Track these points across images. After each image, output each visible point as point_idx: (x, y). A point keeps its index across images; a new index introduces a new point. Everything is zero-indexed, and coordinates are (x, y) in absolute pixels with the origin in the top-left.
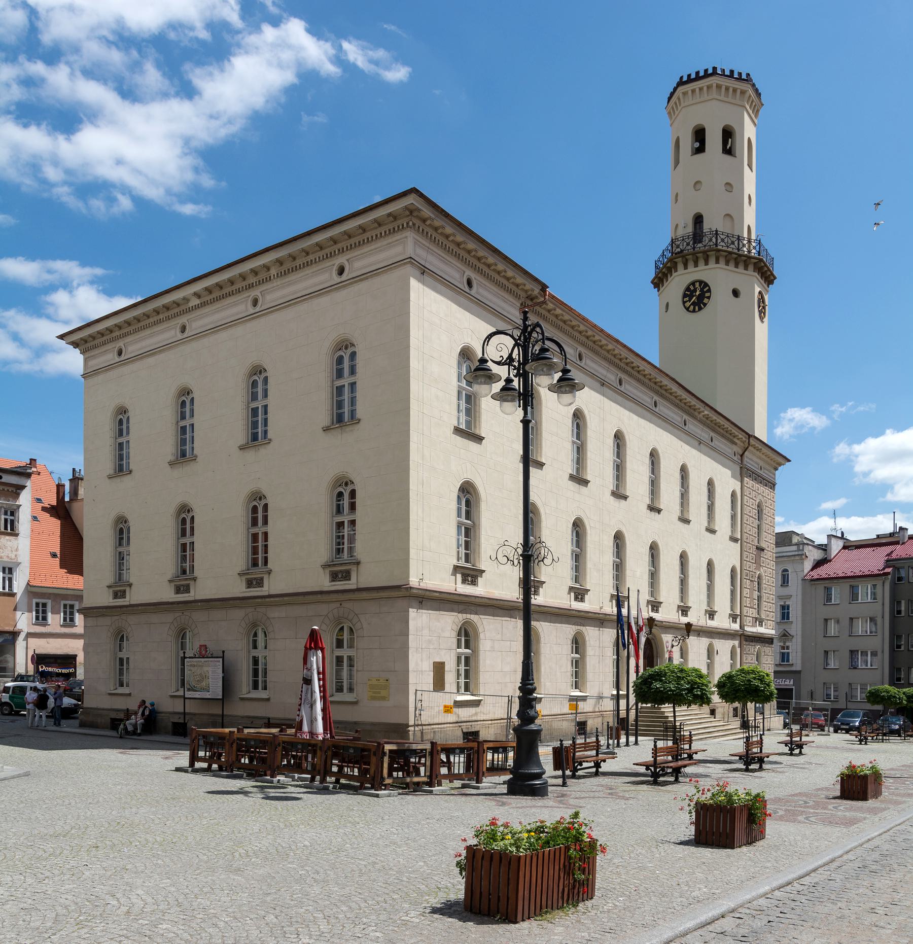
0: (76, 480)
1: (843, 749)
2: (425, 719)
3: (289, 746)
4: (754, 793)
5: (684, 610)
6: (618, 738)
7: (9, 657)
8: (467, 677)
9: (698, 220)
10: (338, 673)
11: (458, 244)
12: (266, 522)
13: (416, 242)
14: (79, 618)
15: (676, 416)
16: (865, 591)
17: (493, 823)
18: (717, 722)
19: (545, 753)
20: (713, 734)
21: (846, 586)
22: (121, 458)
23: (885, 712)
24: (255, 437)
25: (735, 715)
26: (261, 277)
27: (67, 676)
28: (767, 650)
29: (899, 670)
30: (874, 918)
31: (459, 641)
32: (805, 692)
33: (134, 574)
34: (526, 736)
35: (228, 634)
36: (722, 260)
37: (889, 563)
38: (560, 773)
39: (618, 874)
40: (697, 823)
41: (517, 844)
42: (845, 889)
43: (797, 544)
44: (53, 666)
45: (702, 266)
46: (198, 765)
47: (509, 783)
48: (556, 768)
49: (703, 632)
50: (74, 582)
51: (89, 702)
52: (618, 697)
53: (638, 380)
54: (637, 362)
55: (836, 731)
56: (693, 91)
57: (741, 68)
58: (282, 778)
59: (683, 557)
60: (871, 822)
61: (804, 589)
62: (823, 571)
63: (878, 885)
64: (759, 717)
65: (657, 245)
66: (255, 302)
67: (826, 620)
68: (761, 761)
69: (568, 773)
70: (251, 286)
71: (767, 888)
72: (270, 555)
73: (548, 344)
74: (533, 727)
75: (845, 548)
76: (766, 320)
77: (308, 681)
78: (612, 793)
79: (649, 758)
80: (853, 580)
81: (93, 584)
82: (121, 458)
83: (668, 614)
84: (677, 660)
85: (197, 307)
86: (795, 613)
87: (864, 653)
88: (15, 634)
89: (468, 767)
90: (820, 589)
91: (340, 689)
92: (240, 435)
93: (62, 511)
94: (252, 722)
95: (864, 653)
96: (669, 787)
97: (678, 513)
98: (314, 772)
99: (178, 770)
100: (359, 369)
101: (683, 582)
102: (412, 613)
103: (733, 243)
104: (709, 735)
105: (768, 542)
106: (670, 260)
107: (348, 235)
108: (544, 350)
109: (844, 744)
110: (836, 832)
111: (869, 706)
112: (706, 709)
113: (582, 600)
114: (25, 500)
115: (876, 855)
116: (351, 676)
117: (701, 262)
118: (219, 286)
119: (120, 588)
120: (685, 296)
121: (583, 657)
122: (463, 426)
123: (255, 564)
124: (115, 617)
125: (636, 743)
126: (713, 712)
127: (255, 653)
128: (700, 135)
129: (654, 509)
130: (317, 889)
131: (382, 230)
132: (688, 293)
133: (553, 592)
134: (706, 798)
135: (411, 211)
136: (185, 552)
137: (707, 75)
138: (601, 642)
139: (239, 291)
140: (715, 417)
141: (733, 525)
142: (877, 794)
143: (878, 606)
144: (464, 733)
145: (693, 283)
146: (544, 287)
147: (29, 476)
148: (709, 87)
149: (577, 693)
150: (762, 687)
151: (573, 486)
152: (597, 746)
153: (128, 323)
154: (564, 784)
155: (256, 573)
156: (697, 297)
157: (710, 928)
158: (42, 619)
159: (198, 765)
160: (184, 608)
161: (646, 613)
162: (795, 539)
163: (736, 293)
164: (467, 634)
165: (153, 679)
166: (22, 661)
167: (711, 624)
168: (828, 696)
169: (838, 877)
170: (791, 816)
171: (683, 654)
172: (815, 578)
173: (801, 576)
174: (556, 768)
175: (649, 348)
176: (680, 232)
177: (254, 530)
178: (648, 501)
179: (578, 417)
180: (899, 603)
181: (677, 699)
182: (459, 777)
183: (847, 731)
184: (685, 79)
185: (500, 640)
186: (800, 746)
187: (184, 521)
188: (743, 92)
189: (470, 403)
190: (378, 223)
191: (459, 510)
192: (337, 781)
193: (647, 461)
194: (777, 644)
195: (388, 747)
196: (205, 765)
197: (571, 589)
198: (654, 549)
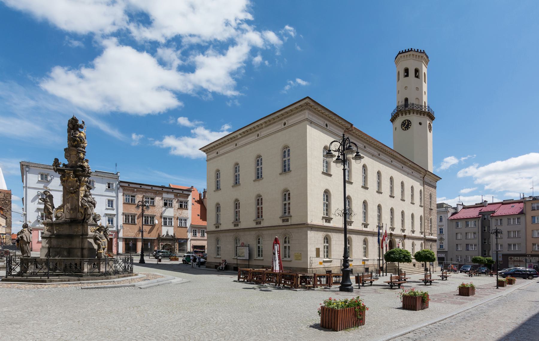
0: (205, 192)
1: (463, 278)
2: (313, 266)
3: (268, 275)
4: (424, 292)
5: (403, 231)
6: (380, 273)
7: (185, 246)
8: (327, 253)
9: (406, 100)
10: (285, 251)
11: (323, 113)
13: (309, 114)
14: (206, 234)
15: (399, 165)
16: (471, 224)
17: (330, 299)
18: (416, 269)
19: (352, 278)
20: (413, 273)
21: (464, 222)
22: (218, 185)
23: (480, 266)
24: (258, 177)
25: (423, 266)
26: (260, 127)
27: (202, 252)
28: (434, 244)
29: (485, 251)
30: (464, 335)
31: (324, 241)
32: (449, 258)
33: (221, 221)
34: (346, 272)
35: (250, 239)
36: (415, 113)
37: (480, 213)
38: (358, 284)
39: (374, 318)
40: (403, 302)
41: (337, 306)
42: (455, 325)
43: (445, 207)
44: (198, 249)
45: (408, 115)
46: (240, 280)
47: (340, 287)
48: (356, 283)
49: (410, 238)
50: (204, 223)
51: (209, 260)
52: (379, 260)
53: (385, 154)
54: (385, 148)
55: (461, 272)
56: (404, 56)
57: (421, 48)
58: (266, 284)
59: (403, 213)
60: (469, 304)
61: (448, 224)
62: (455, 217)
63: (468, 324)
64: (431, 267)
65: (392, 108)
66: (258, 135)
67: (457, 234)
68: (431, 282)
69: (361, 284)
70: (257, 130)
71: (427, 324)
72: (263, 214)
73: (351, 144)
74: (348, 269)
75: (463, 208)
76: (432, 132)
77: (274, 254)
78: (376, 291)
79: (389, 280)
80: (467, 220)
81: (209, 224)
82: (218, 185)
83: (397, 231)
84: (401, 247)
85: (240, 138)
86: (445, 231)
87: (472, 245)
88: (187, 239)
89: (327, 282)
90: (454, 223)
91: (285, 257)
92: (254, 176)
93: (201, 202)
94: (258, 266)
95: (472, 245)
96: (396, 290)
97: (401, 198)
98: (276, 282)
99: (234, 281)
100: (291, 154)
101: (403, 221)
102: (309, 232)
104: (413, 273)
105: (434, 207)
106: (396, 113)
107: (287, 113)
108: (350, 146)
109: (463, 277)
110: (455, 306)
111: (473, 264)
112: (412, 264)
113: (367, 227)
114: (190, 199)
115: (469, 315)
116: (289, 253)
117: (408, 114)
118: (247, 131)
119: (217, 225)
120: (402, 125)
121: (367, 246)
122: (325, 172)
123: (258, 217)
124: (216, 234)
125: (386, 275)
126: (414, 265)
127: (259, 245)
128: (407, 71)
129: (392, 196)
130: (274, 318)
131: (298, 110)
132: (403, 124)
133: (357, 224)
134: (406, 293)
135: (307, 104)
136: (237, 213)
137: (409, 51)
138: (373, 241)
139: (253, 132)
140: (413, 165)
141: (421, 201)
142: (473, 294)
143: (477, 229)
144: (327, 271)
145: (405, 121)
146: (352, 125)
147: (191, 191)
148: (410, 55)
149: (365, 258)
150: (431, 257)
151: (363, 190)
152: (371, 276)
153: (220, 144)
154: (359, 288)
155: (259, 220)
156: (406, 125)
157: (404, 336)
158: (195, 235)
159: (240, 280)
160: (237, 231)
161: (389, 232)
162: (445, 206)
163: (420, 124)
164: (327, 239)
165: (228, 254)
166: (189, 248)
167: (413, 235)
168: (458, 260)
169: (454, 321)
170: (439, 301)
171: (403, 245)
172: (452, 220)
173: (447, 218)
174: (356, 283)
175: (390, 143)
176: (400, 104)
177: (258, 207)
178: (390, 194)
179: (364, 167)
180: (485, 227)
181: (400, 260)
182: (323, 285)
183: (465, 273)
185: (337, 241)
186: (446, 277)
187: (237, 204)
188: (422, 57)
189: (327, 165)
190: (297, 108)
191: (324, 198)
192: (284, 286)
193: (389, 181)
194: (438, 242)
195: (300, 275)
196: (243, 280)
197: (363, 224)
198: (392, 210)
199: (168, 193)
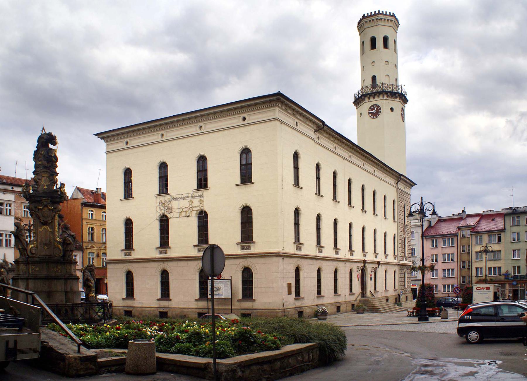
9: (374, 78)
103: (390, 88)
132: (371, 108)
145: (373, 106)
146: (323, 123)
156: (375, 112)
163: (392, 109)
184: (366, 15)
188: (391, 21)
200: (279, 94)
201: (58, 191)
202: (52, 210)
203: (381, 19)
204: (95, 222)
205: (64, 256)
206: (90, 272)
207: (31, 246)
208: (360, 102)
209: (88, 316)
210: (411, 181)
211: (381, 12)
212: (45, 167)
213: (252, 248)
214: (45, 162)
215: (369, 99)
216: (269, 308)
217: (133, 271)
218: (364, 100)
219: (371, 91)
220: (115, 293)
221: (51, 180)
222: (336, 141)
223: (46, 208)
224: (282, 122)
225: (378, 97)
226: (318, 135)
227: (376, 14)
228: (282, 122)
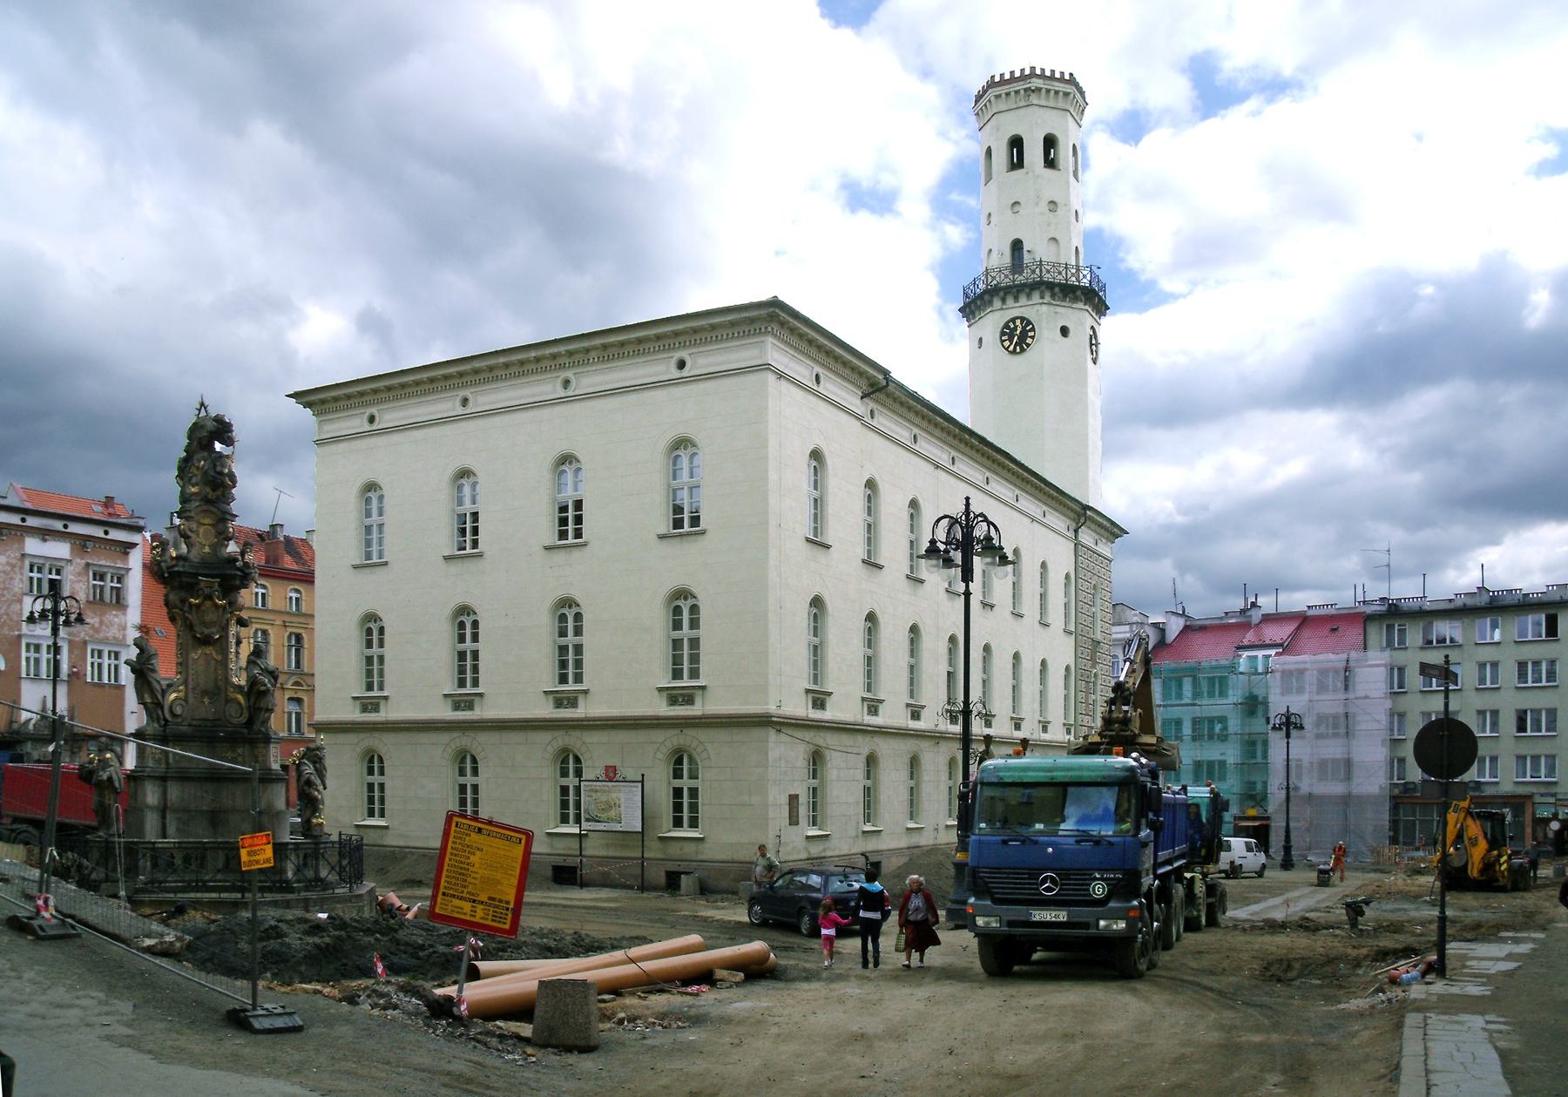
9: (1017, 246)
12: (381, 645)
120: (1003, 334)
128: (1016, 143)
145: (1013, 320)
146: (886, 373)
149: (868, 828)
156: (1018, 337)
163: (1064, 331)
167: (1045, 736)
184: (997, 79)
188: (1066, 94)
199: (45, 534)
200: (775, 303)
201: (236, 560)
202: (224, 607)
203: (1039, 90)
204: (271, 617)
205: (250, 723)
206: (314, 763)
207: (173, 696)
208: (979, 308)
209: (310, 874)
210: (1113, 523)
211: (1038, 72)
212: (207, 501)
213: (698, 701)
214: (208, 489)
215: (1004, 300)
216: (736, 858)
217: (383, 751)
218: (991, 303)
219: (1006, 282)
220: (340, 810)
221: (219, 533)
222: (918, 420)
223: (208, 603)
224: (781, 376)
225: (1029, 296)
226: (872, 405)
227: (1023, 78)
228: (781, 376)
